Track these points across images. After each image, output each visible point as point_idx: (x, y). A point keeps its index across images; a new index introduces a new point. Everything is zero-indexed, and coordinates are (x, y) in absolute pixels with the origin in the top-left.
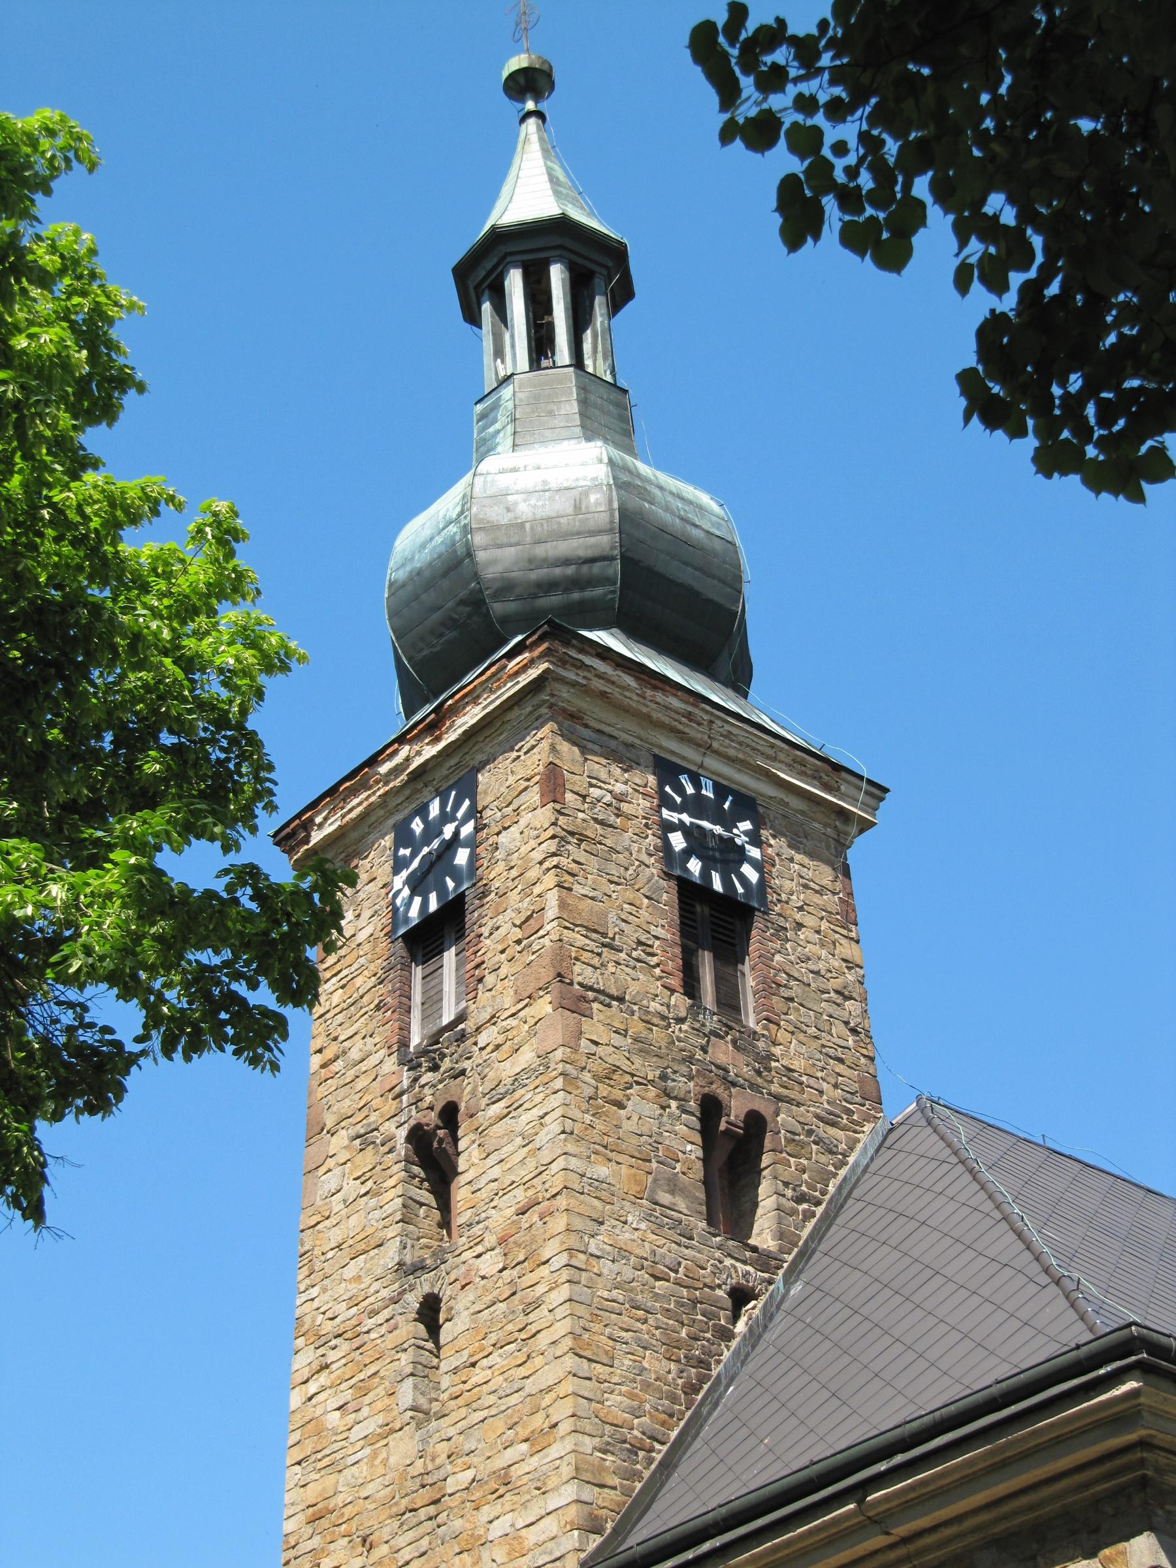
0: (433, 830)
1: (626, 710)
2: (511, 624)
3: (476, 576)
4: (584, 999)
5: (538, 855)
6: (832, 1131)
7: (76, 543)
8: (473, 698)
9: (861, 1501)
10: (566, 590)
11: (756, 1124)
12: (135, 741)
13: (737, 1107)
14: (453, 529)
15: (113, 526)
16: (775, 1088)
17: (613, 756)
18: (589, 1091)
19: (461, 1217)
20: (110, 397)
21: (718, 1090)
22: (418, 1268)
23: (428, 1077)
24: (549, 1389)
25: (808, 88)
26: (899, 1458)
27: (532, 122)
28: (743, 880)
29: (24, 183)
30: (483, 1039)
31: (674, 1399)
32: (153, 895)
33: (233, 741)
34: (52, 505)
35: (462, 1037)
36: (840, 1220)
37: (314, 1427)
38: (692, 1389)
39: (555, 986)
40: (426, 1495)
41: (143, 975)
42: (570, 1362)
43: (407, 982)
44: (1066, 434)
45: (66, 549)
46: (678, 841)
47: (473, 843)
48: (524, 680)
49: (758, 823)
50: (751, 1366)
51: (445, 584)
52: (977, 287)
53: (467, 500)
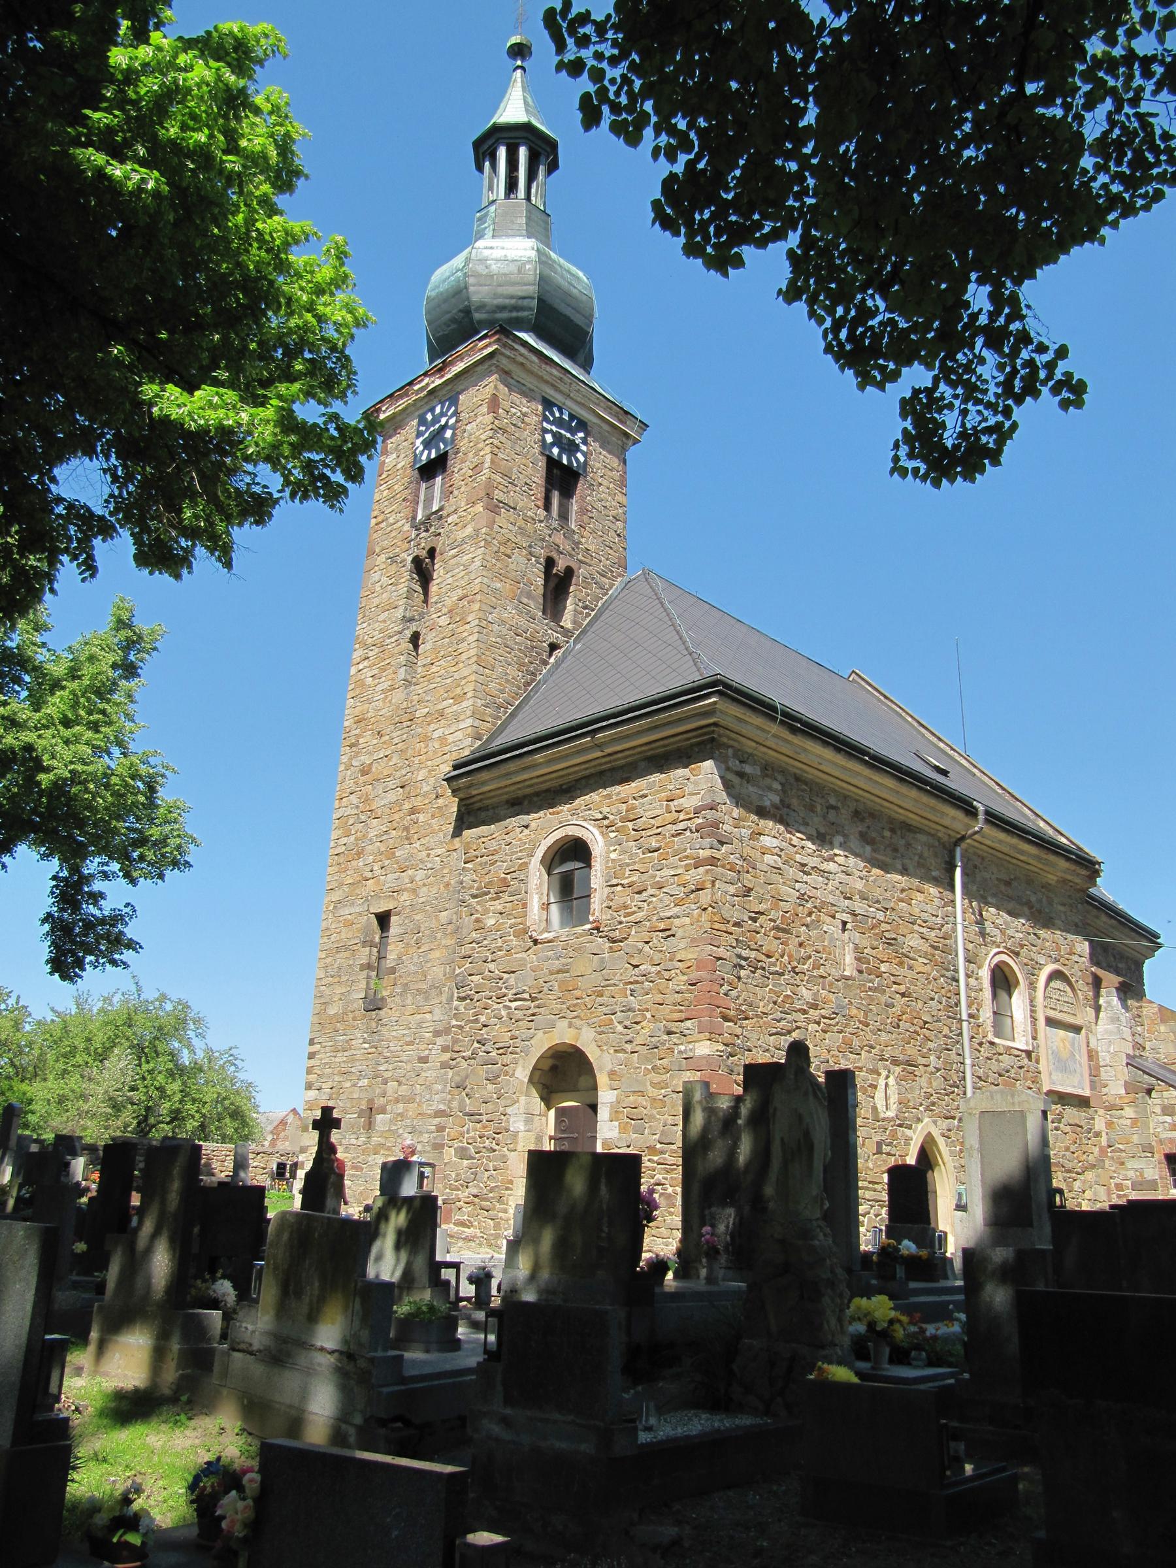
0: (436, 420)
1: (531, 373)
2: (484, 324)
3: (468, 299)
4: (497, 506)
5: (483, 437)
6: (603, 579)
7: (268, 251)
8: (461, 358)
9: (593, 737)
10: (511, 311)
11: (569, 572)
12: (292, 354)
13: (561, 565)
14: (459, 274)
15: (286, 245)
16: (580, 557)
17: (523, 394)
18: (496, 549)
19: (432, 600)
20: (291, 180)
21: (554, 555)
22: (412, 620)
23: (424, 535)
24: (465, 678)
25: (600, 48)
26: (612, 721)
27: (519, 71)
28: (577, 460)
29: (250, 59)
30: (450, 520)
31: (519, 688)
32: (288, 423)
33: (339, 359)
34: (257, 230)
35: (441, 518)
36: (602, 618)
37: (361, 683)
38: (527, 684)
39: (485, 499)
40: (408, 717)
41: (283, 461)
42: (475, 667)
43: (418, 490)
44: (698, 239)
45: (263, 254)
46: (549, 438)
47: (454, 428)
48: (485, 352)
49: (587, 434)
50: (554, 677)
51: (453, 301)
52: (662, 158)
53: (468, 260)
